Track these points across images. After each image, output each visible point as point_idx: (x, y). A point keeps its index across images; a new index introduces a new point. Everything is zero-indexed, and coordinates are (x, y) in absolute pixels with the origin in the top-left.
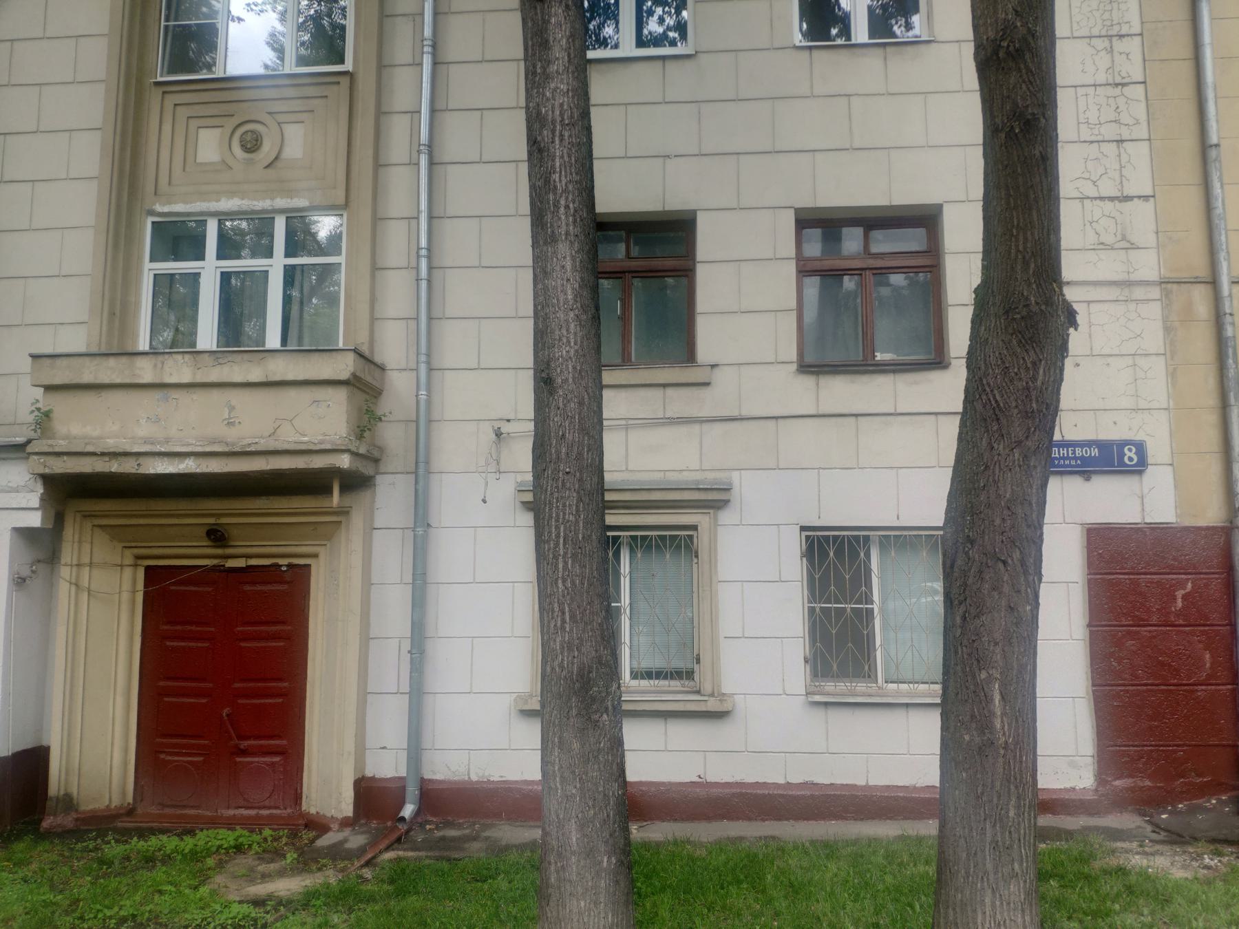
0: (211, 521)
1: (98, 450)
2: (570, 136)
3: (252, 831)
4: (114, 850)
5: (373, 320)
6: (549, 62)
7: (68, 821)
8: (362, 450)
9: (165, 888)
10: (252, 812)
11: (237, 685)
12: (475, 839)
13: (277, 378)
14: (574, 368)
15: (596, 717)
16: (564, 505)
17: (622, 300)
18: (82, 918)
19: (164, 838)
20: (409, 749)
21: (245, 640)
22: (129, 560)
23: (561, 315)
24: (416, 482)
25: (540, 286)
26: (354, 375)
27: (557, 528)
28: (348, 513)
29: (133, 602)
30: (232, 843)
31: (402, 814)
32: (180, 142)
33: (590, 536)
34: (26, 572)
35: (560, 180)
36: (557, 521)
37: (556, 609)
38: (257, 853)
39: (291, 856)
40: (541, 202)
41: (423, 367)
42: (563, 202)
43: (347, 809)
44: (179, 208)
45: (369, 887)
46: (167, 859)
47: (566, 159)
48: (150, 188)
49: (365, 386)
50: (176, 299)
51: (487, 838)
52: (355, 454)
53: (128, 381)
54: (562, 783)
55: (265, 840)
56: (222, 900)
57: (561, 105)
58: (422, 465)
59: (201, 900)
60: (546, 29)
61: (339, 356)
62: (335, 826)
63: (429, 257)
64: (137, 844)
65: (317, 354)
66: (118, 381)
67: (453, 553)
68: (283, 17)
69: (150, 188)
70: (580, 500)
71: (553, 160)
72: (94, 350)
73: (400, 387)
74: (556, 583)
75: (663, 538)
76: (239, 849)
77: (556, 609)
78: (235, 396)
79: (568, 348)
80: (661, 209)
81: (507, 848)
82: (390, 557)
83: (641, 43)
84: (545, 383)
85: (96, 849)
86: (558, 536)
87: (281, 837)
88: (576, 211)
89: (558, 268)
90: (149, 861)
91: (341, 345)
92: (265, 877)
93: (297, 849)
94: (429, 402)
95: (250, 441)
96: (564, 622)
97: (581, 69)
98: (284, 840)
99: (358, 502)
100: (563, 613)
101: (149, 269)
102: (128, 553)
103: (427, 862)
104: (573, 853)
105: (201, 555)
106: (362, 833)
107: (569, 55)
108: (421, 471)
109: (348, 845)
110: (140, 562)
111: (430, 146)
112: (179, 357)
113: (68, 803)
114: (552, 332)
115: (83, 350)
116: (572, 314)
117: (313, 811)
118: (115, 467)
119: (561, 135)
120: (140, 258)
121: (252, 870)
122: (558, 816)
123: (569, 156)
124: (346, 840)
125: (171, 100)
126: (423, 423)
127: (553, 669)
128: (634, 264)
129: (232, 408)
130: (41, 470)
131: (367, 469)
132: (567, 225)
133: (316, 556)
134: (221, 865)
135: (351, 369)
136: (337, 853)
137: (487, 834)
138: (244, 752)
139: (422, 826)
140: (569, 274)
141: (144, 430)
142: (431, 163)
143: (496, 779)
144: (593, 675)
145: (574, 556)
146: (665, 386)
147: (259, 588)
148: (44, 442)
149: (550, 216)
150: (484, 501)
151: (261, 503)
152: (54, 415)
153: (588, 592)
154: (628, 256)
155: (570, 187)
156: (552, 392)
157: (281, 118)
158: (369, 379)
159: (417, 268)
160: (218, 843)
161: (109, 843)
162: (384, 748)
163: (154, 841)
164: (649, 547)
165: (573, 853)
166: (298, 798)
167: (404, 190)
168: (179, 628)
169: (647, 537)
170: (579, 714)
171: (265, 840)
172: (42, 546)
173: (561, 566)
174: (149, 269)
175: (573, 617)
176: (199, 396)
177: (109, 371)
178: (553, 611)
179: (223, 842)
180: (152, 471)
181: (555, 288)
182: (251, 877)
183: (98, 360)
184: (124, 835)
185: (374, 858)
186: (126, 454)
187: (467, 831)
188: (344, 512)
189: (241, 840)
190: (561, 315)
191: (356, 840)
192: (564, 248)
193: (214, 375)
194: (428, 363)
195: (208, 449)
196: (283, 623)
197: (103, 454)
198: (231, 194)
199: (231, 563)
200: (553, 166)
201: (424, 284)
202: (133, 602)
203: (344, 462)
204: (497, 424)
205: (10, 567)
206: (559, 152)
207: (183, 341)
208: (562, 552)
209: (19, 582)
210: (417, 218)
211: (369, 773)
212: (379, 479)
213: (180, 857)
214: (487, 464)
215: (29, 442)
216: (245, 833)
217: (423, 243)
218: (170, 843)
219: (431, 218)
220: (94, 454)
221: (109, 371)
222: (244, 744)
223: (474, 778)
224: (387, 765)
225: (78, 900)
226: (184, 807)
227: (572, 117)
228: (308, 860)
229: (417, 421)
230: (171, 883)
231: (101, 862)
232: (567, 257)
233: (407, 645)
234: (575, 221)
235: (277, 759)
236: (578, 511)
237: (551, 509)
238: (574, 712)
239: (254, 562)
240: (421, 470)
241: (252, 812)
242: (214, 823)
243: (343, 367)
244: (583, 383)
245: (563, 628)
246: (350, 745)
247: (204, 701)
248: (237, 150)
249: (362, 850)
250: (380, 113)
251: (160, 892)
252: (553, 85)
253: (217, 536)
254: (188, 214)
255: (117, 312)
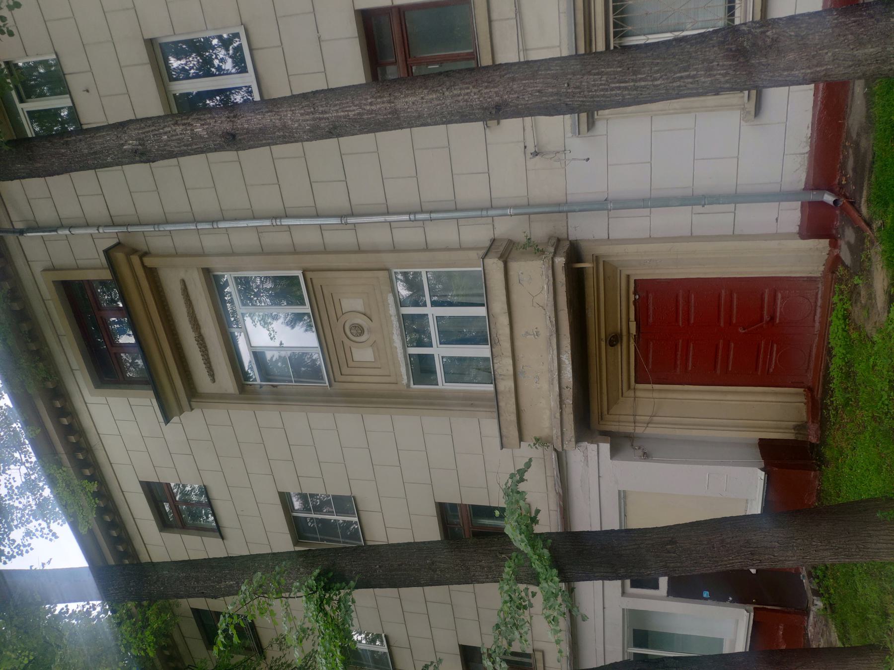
0: (603, 344)
1: (559, 411)
2: (322, 106)
3: (833, 309)
4: (838, 397)
5: (461, 248)
6: (275, 126)
7: (813, 429)
8: (552, 250)
9: (871, 363)
10: (819, 310)
11: (722, 324)
12: (857, 144)
13: (506, 307)
14: (486, 87)
15: (769, 40)
16: (594, 85)
17: (428, 65)
18: (886, 414)
19: (832, 367)
20: (780, 201)
21: (689, 320)
22: (631, 393)
23: (448, 102)
24: (574, 211)
25: (429, 120)
26: (500, 258)
27: (612, 89)
28: (597, 257)
29: (660, 391)
30: (841, 322)
31: (831, 203)
32: (363, 371)
33: (619, 62)
34: (640, 452)
35: (353, 111)
36: (607, 90)
37: (678, 83)
38: (851, 305)
39: (857, 280)
40: (370, 124)
41: (491, 213)
42: (368, 107)
43: (825, 242)
44: (403, 370)
45: (889, 221)
46: (849, 364)
47: (337, 108)
48: (393, 387)
49: (505, 251)
50: (458, 369)
51: (858, 135)
52: (555, 254)
53: (513, 395)
54: (821, 66)
55: (841, 300)
56: (886, 324)
57: (302, 115)
58: (561, 209)
59: (883, 339)
60: (253, 130)
61: (488, 268)
62: (836, 252)
63: (415, 213)
64: (835, 384)
65: (488, 283)
66: (514, 400)
67: (627, 181)
68: (276, 318)
69: (393, 387)
70: (589, 73)
71: (340, 117)
72: (496, 415)
73: (507, 227)
74: (657, 86)
75: (615, 9)
76: (847, 317)
77: (678, 83)
78: (519, 331)
79: (472, 94)
80: (357, 40)
81: (869, 117)
82: (630, 224)
83: (243, 70)
84: (499, 110)
85: (836, 409)
86: (619, 88)
87: (840, 290)
88: (373, 97)
89: (415, 107)
90: (849, 374)
91: (481, 269)
92: (871, 296)
93: (851, 277)
94: (515, 207)
95: (548, 322)
96: (688, 77)
97: (271, 104)
98: (843, 287)
99: (588, 250)
100: (682, 77)
101: (442, 385)
102: (625, 394)
103: (873, 179)
104: (884, 49)
105: (628, 351)
106: (843, 231)
107: (267, 112)
108: (565, 208)
109: (852, 241)
110: (632, 387)
111: (341, 217)
112: (496, 366)
113: (800, 428)
114: (461, 107)
115: (496, 421)
116: (447, 93)
117: (822, 268)
118: (569, 401)
119: (322, 113)
120: (436, 391)
121: (864, 307)
122: (850, 66)
123: (336, 105)
124: (848, 244)
125: (339, 377)
126: (528, 209)
127: (727, 82)
128: (400, 58)
129: (527, 333)
130: (573, 443)
131: (565, 246)
132: (383, 103)
133: (628, 276)
134: (858, 328)
135: (496, 260)
136: (857, 249)
137: (854, 136)
138: (773, 318)
139: (842, 187)
140: (418, 98)
141: (544, 385)
142: (353, 215)
143: (809, 132)
144: (733, 47)
145: (635, 73)
146: (490, 21)
147: (651, 312)
148: (554, 441)
149: (379, 117)
150: (588, 159)
151: (591, 314)
152: (538, 436)
153: (665, 59)
154: (395, 63)
155: (357, 102)
156: (506, 104)
157: (339, 314)
158: (502, 249)
159: (423, 220)
160: (840, 331)
161: (832, 402)
162: (777, 219)
163: (834, 373)
164: (623, 20)
165: (884, 49)
166: (811, 280)
167: (374, 233)
168: (679, 362)
169: (614, 23)
170: (765, 56)
171: (841, 300)
172: (620, 443)
173: (643, 83)
174: (442, 385)
175: (685, 69)
176: (520, 354)
177: (508, 405)
178: (679, 86)
179: (840, 328)
180: (571, 380)
181: (429, 108)
182: (869, 307)
183: (501, 412)
184: (827, 391)
185: (865, 221)
186: (560, 395)
187: (851, 151)
188: (596, 259)
189: (840, 316)
190: (448, 102)
191: (850, 235)
192: (400, 104)
193: (506, 345)
194: (487, 209)
195: (555, 347)
196: (677, 296)
197: (561, 408)
198: (391, 341)
199: (633, 330)
200: (345, 117)
201: (434, 216)
202: (660, 391)
203: (560, 261)
204: (529, 156)
205: (635, 460)
206: (334, 113)
207: (485, 370)
208: (632, 84)
209: (646, 456)
210: (390, 222)
211: (796, 229)
212: (572, 238)
213: (848, 356)
214: (559, 160)
215: (555, 450)
216: (834, 314)
217: (406, 217)
218: (837, 362)
219: (388, 213)
220: (561, 414)
221: (508, 405)
222: (766, 317)
223: (807, 149)
224: (791, 216)
225: (873, 417)
226: (810, 355)
227: (308, 106)
228: (862, 269)
229: (529, 214)
230: (868, 360)
231: (846, 404)
232: (408, 101)
233: (698, 208)
234: (380, 97)
235: (779, 296)
236: (598, 74)
237: (598, 96)
238: (764, 60)
239: (632, 317)
240: (563, 209)
241: (819, 310)
242: (824, 335)
243: (495, 266)
244: (497, 79)
245: (693, 77)
246: (773, 244)
247: (732, 345)
248: (363, 338)
249: (859, 231)
250: (325, 251)
251: (874, 365)
252: (290, 123)
253: (614, 340)
254: (407, 365)
255: (470, 402)
